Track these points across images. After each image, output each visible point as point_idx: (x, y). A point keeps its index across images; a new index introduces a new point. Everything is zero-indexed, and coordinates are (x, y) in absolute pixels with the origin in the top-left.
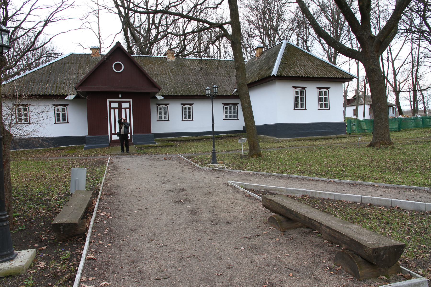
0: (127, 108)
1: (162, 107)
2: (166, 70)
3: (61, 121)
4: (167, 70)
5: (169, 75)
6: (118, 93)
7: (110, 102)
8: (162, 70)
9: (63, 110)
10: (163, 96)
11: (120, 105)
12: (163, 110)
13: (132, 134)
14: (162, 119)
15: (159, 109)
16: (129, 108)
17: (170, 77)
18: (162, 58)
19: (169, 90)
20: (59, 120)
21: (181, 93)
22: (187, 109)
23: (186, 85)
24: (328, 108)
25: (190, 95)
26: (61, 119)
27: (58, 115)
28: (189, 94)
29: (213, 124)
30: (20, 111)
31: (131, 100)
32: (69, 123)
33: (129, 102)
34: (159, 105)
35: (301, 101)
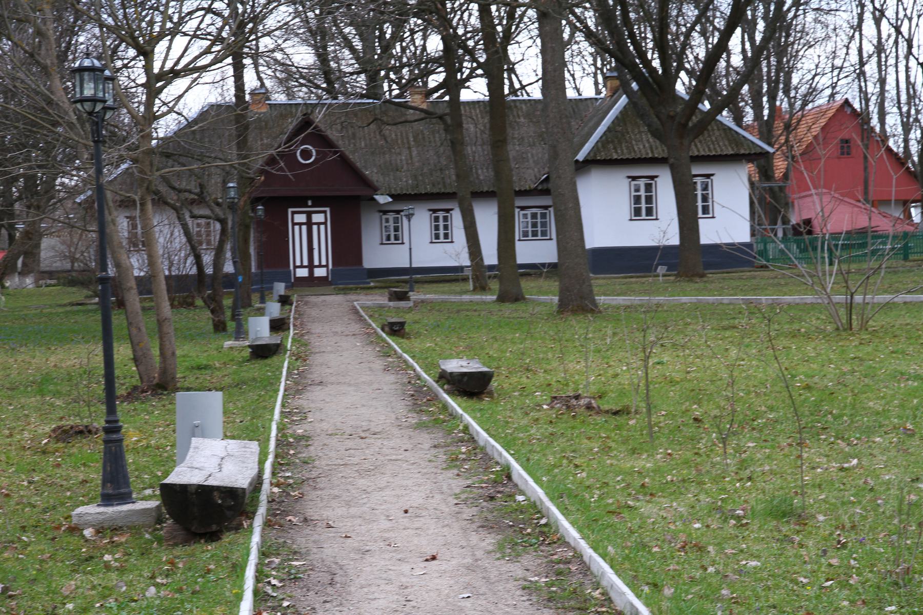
0: (299, 267)
1: (391, 216)
2: (404, 134)
4: (407, 135)
5: (409, 148)
6: (306, 198)
7: (293, 213)
8: (396, 135)
10: (391, 196)
11: (311, 272)
12: (391, 224)
13: (330, 267)
14: (528, 236)
15: (384, 221)
16: (325, 223)
17: (410, 152)
19: (405, 184)
20: (437, 237)
21: (426, 188)
22: (441, 219)
23: (441, 170)
24: (710, 215)
25: (443, 193)
26: (442, 236)
28: (443, 190)
29: (410, 249)
31: (328, 209)
33: (325, 212)
34: (385, 212)
35: (647, 203)
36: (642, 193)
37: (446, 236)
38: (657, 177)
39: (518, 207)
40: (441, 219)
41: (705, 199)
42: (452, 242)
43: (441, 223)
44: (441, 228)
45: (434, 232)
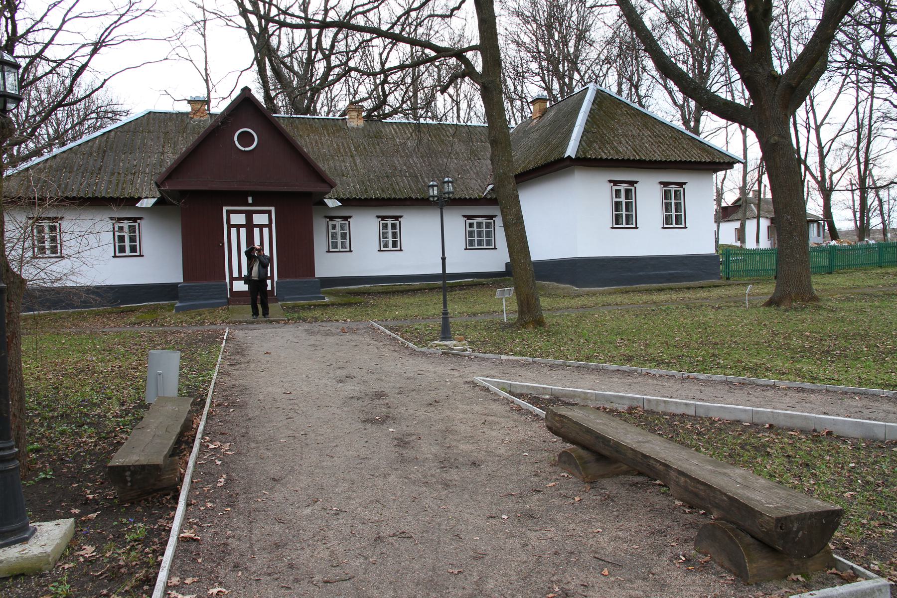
0: (265, 226)
1: (338, 223)
2: (345, 145)
3: (128, 253)
4: (348, 145)
5: (352, 156)
6: (246, 194)
7: (229, 213)
8: (338, 145)
9: (132, 229)
10: (340, 200)
11: (249, 219)
12: (338, 230)
13: (276, 279)
14: (337, 248)
15: (330, 227)
16: (269, 226)
17: (354, 160)
18: (336, 121)
19: (351, 187)
20: (122, 249)
21: (376, 194)
22: (390, 226)
23: (387, 177)
24: (683, 226)
25: (395, 199)
26: (128, 249)
27: (121, 239)
28: (394, 196)
29: (444, 259)
30: (41, 231)
31: (273, 209)
32: (143, 256)
33: (269, 212)
34: (332, 218)
35: (627, 210)
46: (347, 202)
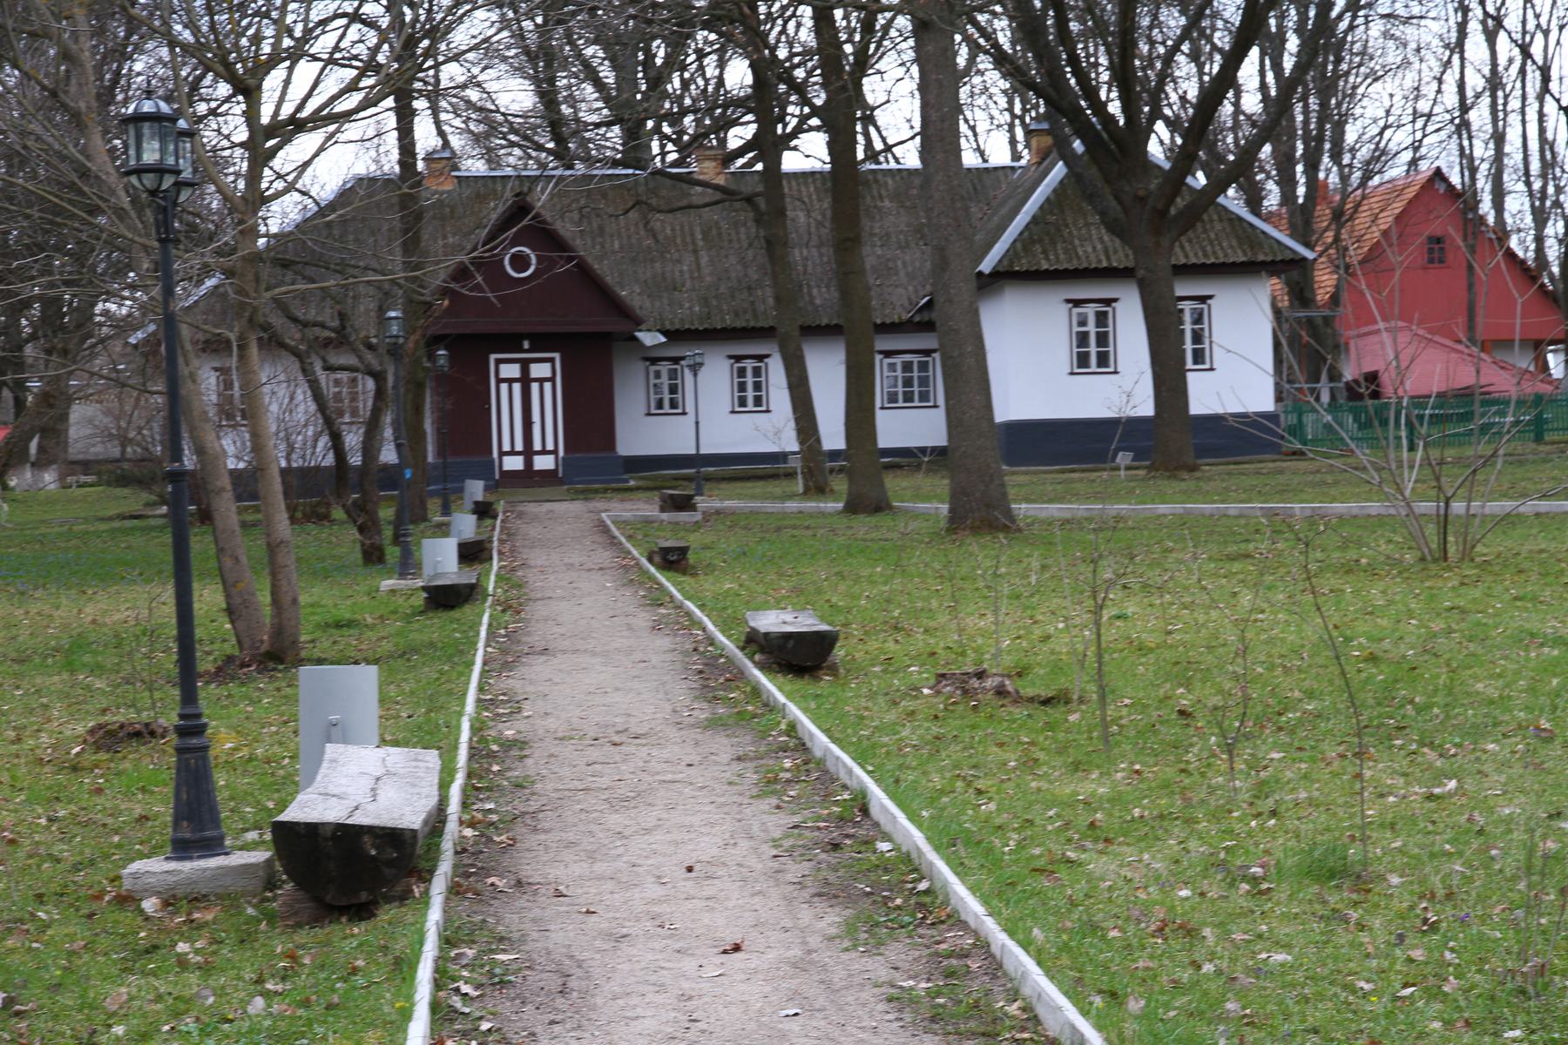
0: (508, 454)
1: (664, 368)
2: (687, 228)
3: (750, 407)
4: (691, 229)
5: (695, 251)
6: (521, 337)
7: (499, 362)
8: (673, 230)
10: (665, 333)
11: (529, 463)
12: (665, 380)
13: (561, 453)
14: (896, 402)
15: (652, 375)
16: (552, 379)
17: (697, 259)
19: (687, 312)
20: (743, 402)
21: (723, 320)
22: (749, 372)
23: (749, 288)
24: (1207, 366)
25: (753, 328)
26: (750, 401)
28: (752, 324)
29: (697, 423)
31: (557, 356)
33: (552, 360)
34: (654, 361)
35: (1099, 344)
36: (1091, 328)
37: (758, 401)
38: (1115, 300)
39: (880, 352)
40: (749, 372)
41: (1197, 337)
42: (768, 411)
43: (750, 380)
44: (750, 387)
45: (737, 394)
46: (674, 336)
